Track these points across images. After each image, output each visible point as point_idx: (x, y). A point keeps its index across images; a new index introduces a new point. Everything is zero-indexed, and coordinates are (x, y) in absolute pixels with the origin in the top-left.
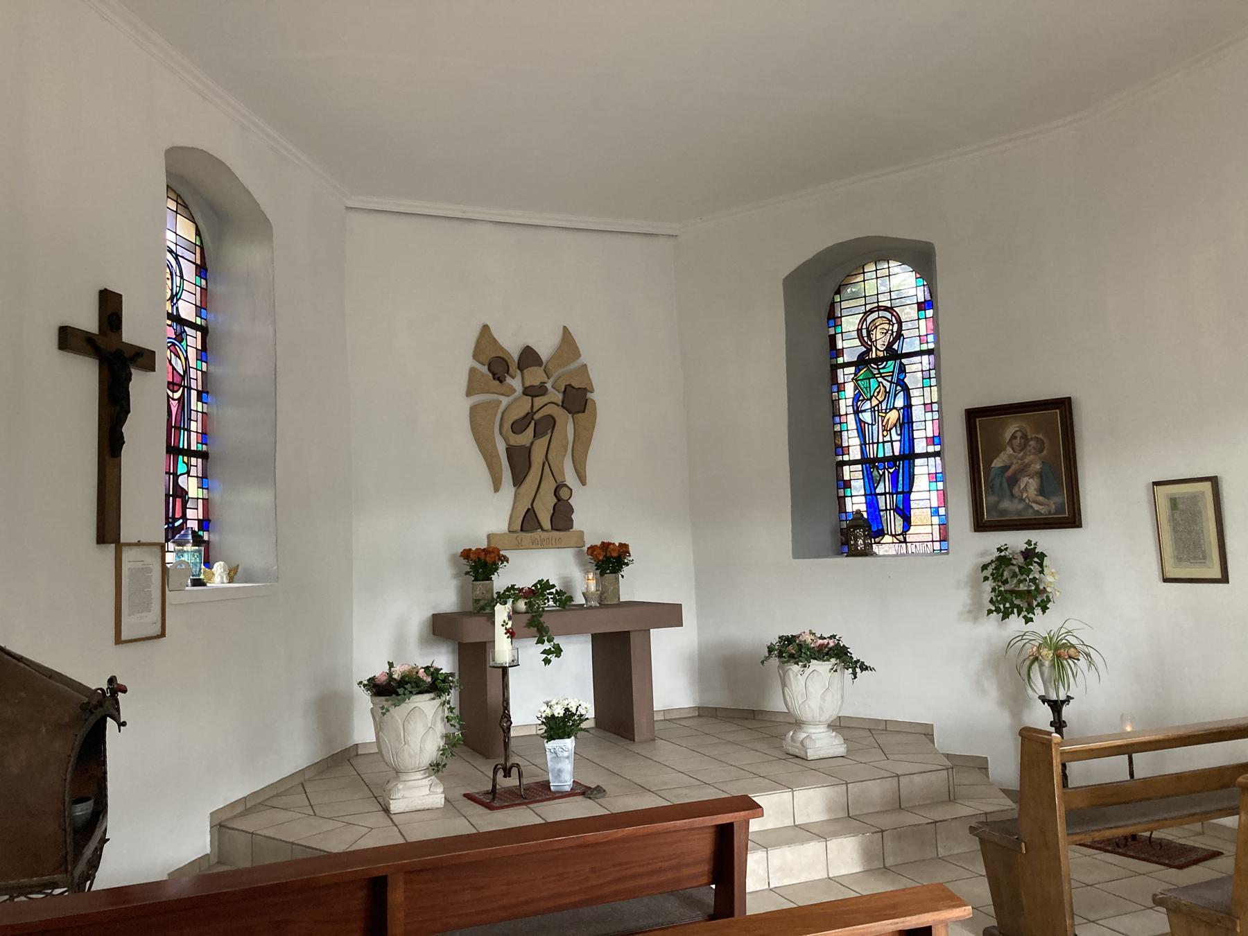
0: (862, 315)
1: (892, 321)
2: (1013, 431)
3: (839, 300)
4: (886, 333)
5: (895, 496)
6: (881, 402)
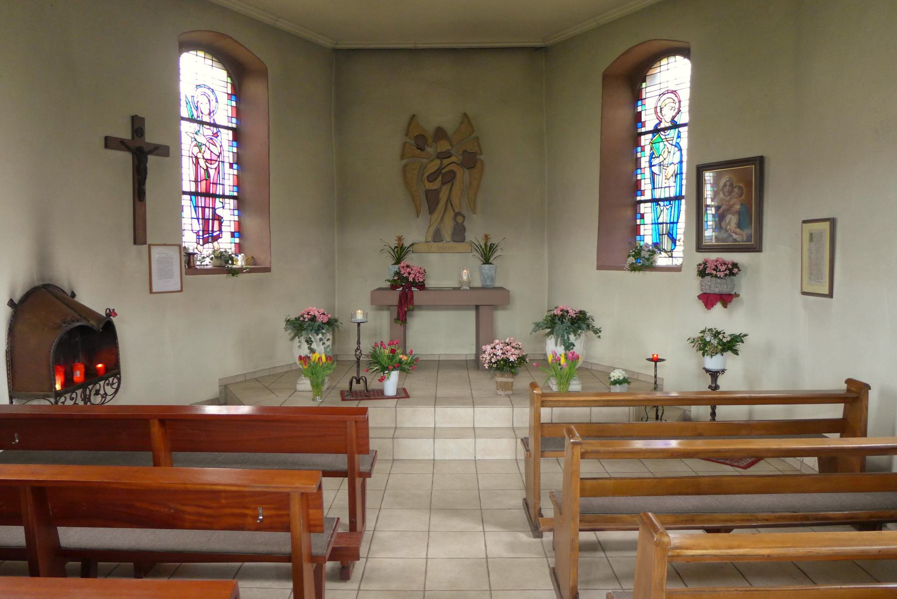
2: (725, 181)
3: (645, 87)
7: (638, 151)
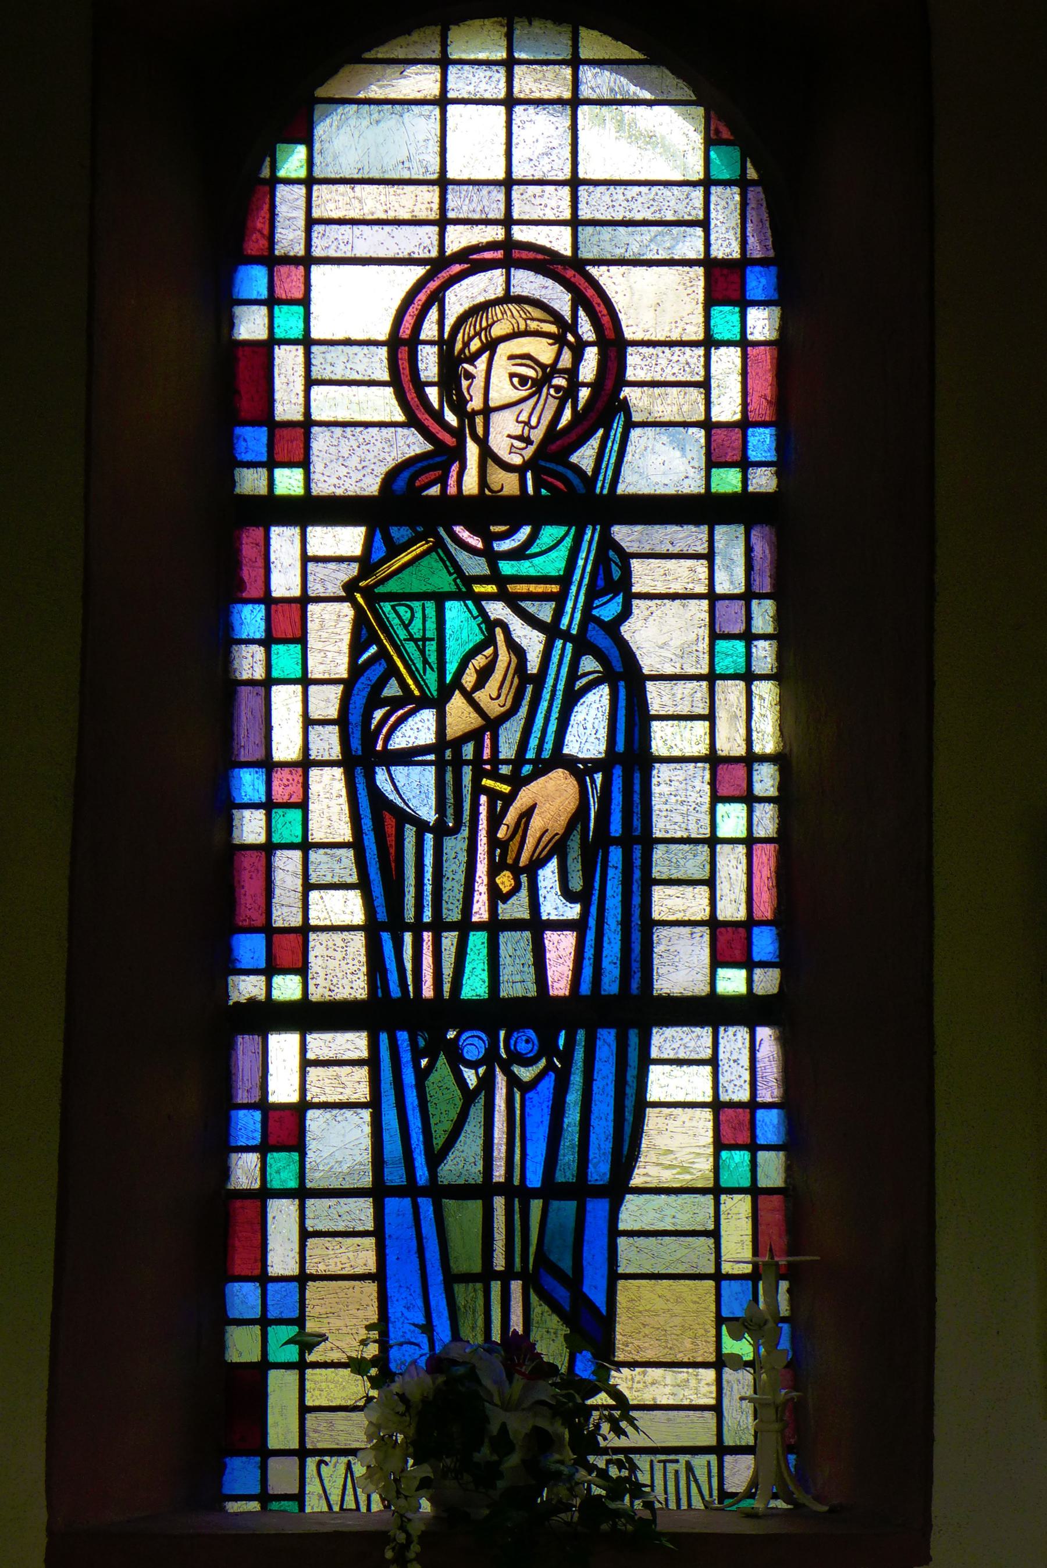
0: (420, 271)
1: (573, 328)
4: (539, 385)
5: (536, 1206)
6: (493, 725)
7: (770, 848)
